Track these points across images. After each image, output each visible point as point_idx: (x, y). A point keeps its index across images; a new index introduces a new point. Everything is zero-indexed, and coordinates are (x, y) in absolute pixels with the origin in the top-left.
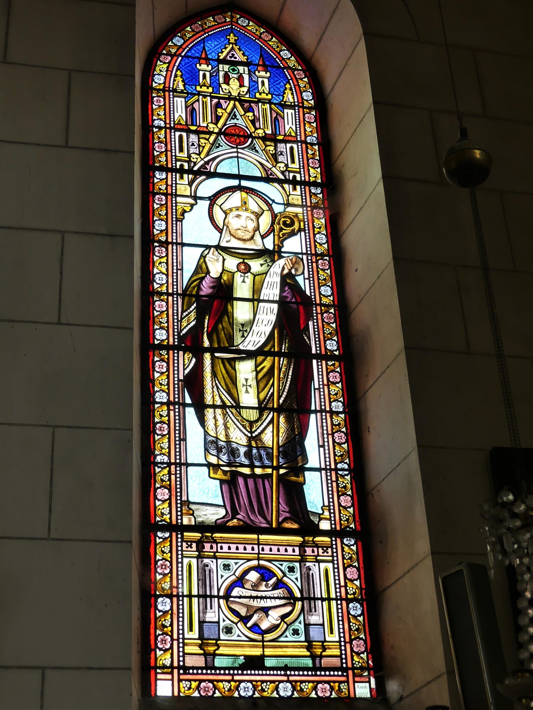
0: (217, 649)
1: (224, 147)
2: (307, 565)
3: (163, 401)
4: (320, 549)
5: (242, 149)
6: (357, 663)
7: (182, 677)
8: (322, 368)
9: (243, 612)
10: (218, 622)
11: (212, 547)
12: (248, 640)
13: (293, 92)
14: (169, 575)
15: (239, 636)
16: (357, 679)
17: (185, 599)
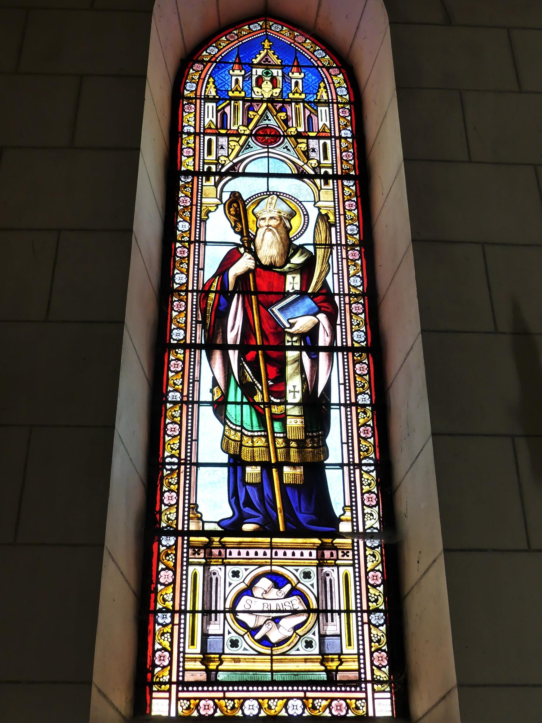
7: (181, 695)
10: (223, 635)
13: (327, 90)
14: (179, 437)
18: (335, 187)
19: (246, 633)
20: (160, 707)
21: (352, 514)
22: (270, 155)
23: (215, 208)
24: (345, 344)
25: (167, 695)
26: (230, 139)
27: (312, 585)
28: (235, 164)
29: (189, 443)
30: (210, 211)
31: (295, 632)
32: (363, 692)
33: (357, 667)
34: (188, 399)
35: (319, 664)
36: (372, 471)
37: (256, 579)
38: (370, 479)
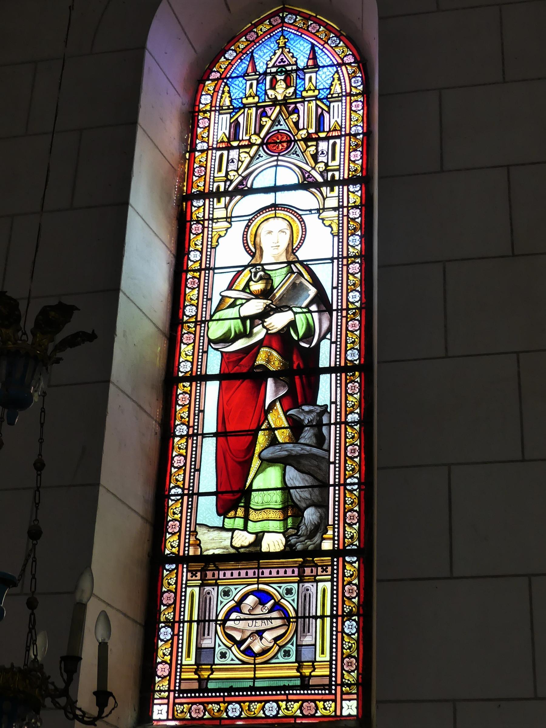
0: (212, 674)
1: (264, 157)
2: (305, 586)
3: (183, 434)
4: (319, 568)
5: (282, 156)
6: (347, 644)
7: (177, 701)
8: (342, 277)
9: (238, 637)
10: (214, 648)
11: (214, 575)
12: (240, 663)
13: (341, 82)
14: (168, 678)
15: (232, 660)
16: (344, 697)
17: (186, 624)
18: (342, 163)
19: (233, 645)
20: (159, 712)
21: (334, 532)
22: (279, 163)
23: (225, 232)
24: (335, 560)
25: (166, 701)
26: (241, 150)
27: (293, 600)
28: (245, 178)
29: (192, 474)
30: (220, 236)
31: (275, 643)
32: (333, 694)
33: (328, 673)
34: (189, 492)
35: (295, 671)
36: (355, 562)
37: (245, 597)
38: (352, 570)
